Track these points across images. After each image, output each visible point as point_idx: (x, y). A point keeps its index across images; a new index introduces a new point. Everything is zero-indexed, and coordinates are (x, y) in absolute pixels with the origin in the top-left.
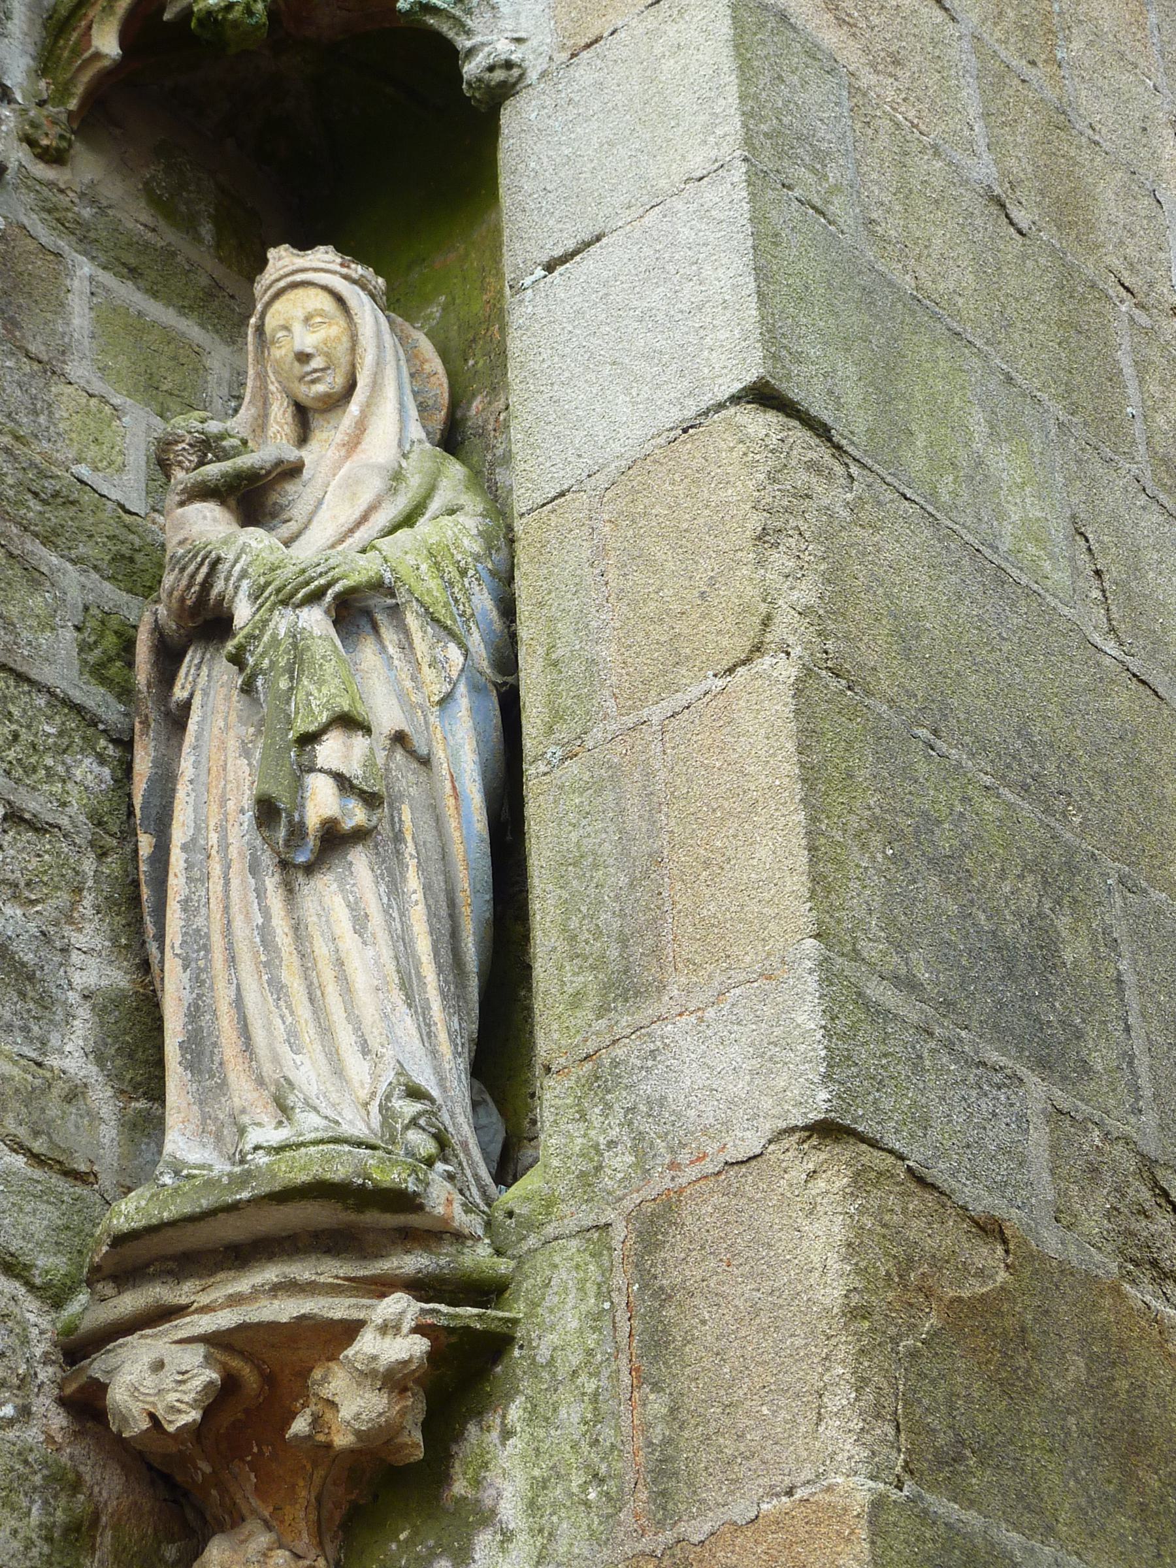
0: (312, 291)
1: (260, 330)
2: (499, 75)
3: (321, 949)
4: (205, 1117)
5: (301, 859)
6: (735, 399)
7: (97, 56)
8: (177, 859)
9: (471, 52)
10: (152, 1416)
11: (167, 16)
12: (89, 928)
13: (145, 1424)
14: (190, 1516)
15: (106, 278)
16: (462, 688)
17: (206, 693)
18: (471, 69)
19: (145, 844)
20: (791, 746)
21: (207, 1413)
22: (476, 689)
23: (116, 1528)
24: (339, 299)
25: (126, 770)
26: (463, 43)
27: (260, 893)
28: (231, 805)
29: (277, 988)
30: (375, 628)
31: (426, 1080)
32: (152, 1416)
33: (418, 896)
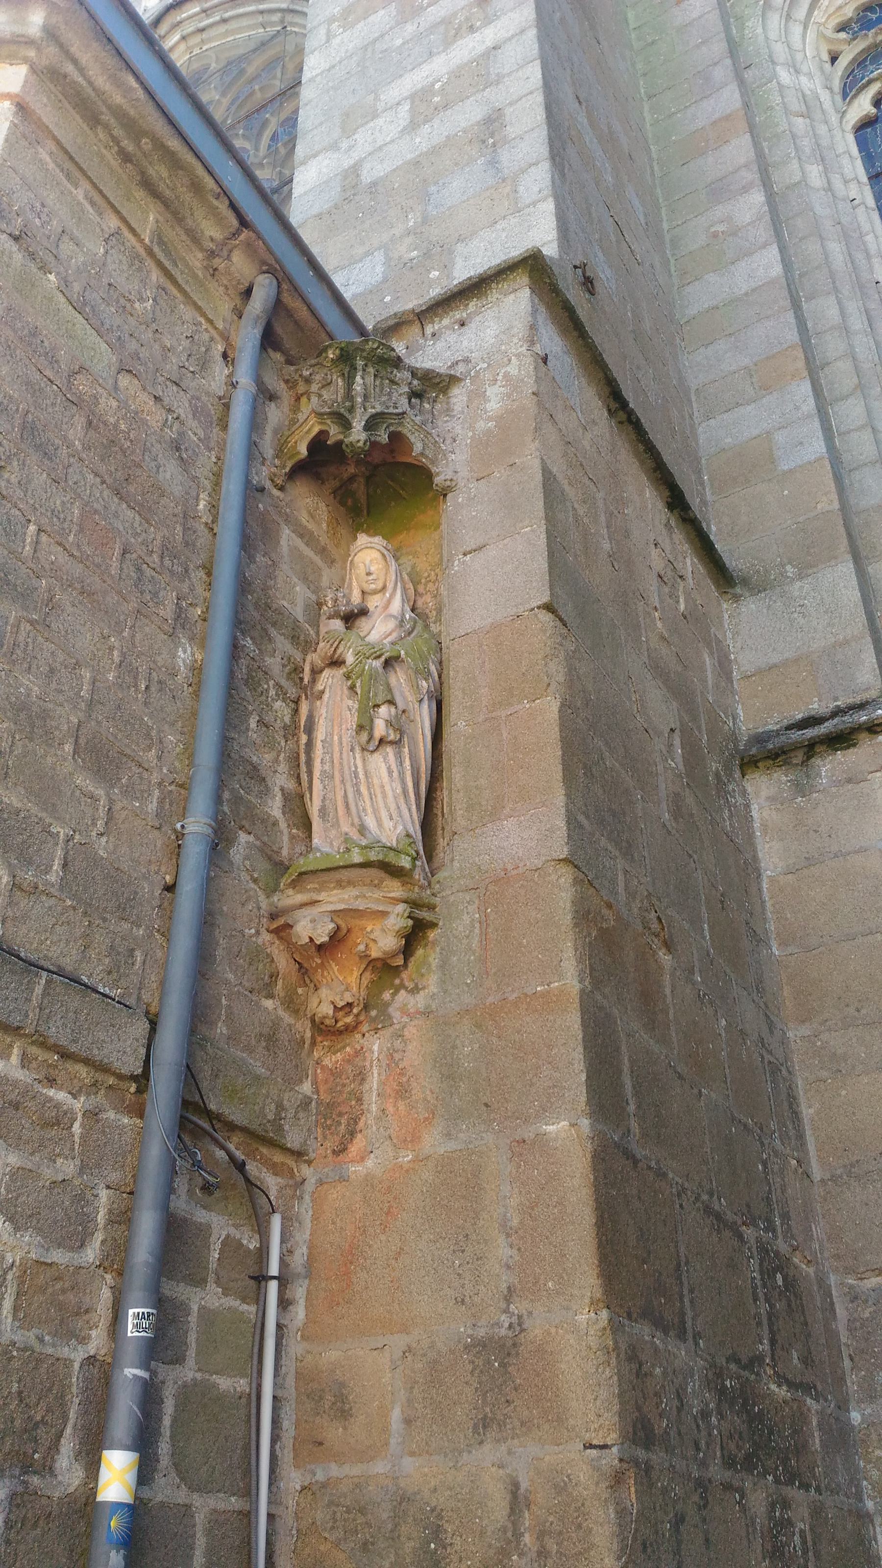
0: (374, 551)
1: (352, 561)
2: (448, 483)
3: (376, 781)
4: (326, 836)
5: (371, 749)
6: (539, 607)
7: (298, 453)
8: (319, 745)
9: (438, 474)
10: (311, 938)
11: (328, 443)
12: (282, 766)
13: (308, 940)
14: (306, 979)
15: (293, 535)
16: (426, 697)
17: (330, 688)
18: (437, 480)
19: (304, 738)
20: (557, 729)
21: (331, 938)
22: (430, 699)
23: (284, 980)
24: (383, 555)
25: (296, 711)
26: (434, 469)
27: (355, 758)
28: (344, 726)
29: (358, 792)
30: (396, 672)
31: (411, 831)
32: (311, 938)
33: (409, 768)
